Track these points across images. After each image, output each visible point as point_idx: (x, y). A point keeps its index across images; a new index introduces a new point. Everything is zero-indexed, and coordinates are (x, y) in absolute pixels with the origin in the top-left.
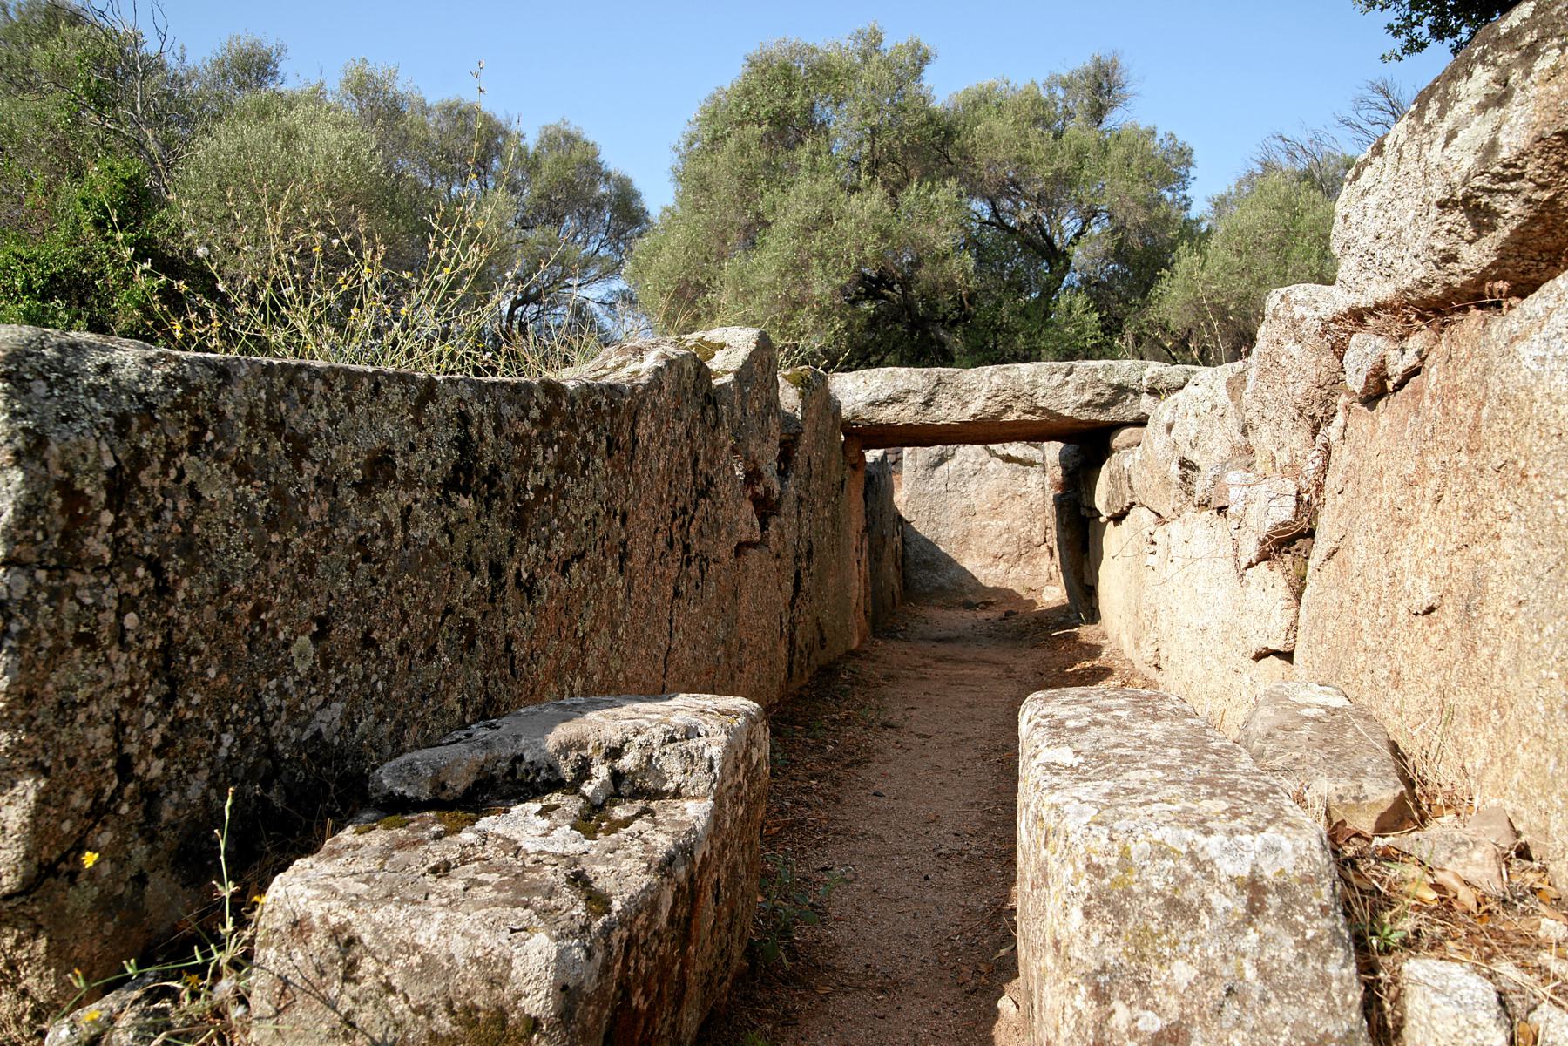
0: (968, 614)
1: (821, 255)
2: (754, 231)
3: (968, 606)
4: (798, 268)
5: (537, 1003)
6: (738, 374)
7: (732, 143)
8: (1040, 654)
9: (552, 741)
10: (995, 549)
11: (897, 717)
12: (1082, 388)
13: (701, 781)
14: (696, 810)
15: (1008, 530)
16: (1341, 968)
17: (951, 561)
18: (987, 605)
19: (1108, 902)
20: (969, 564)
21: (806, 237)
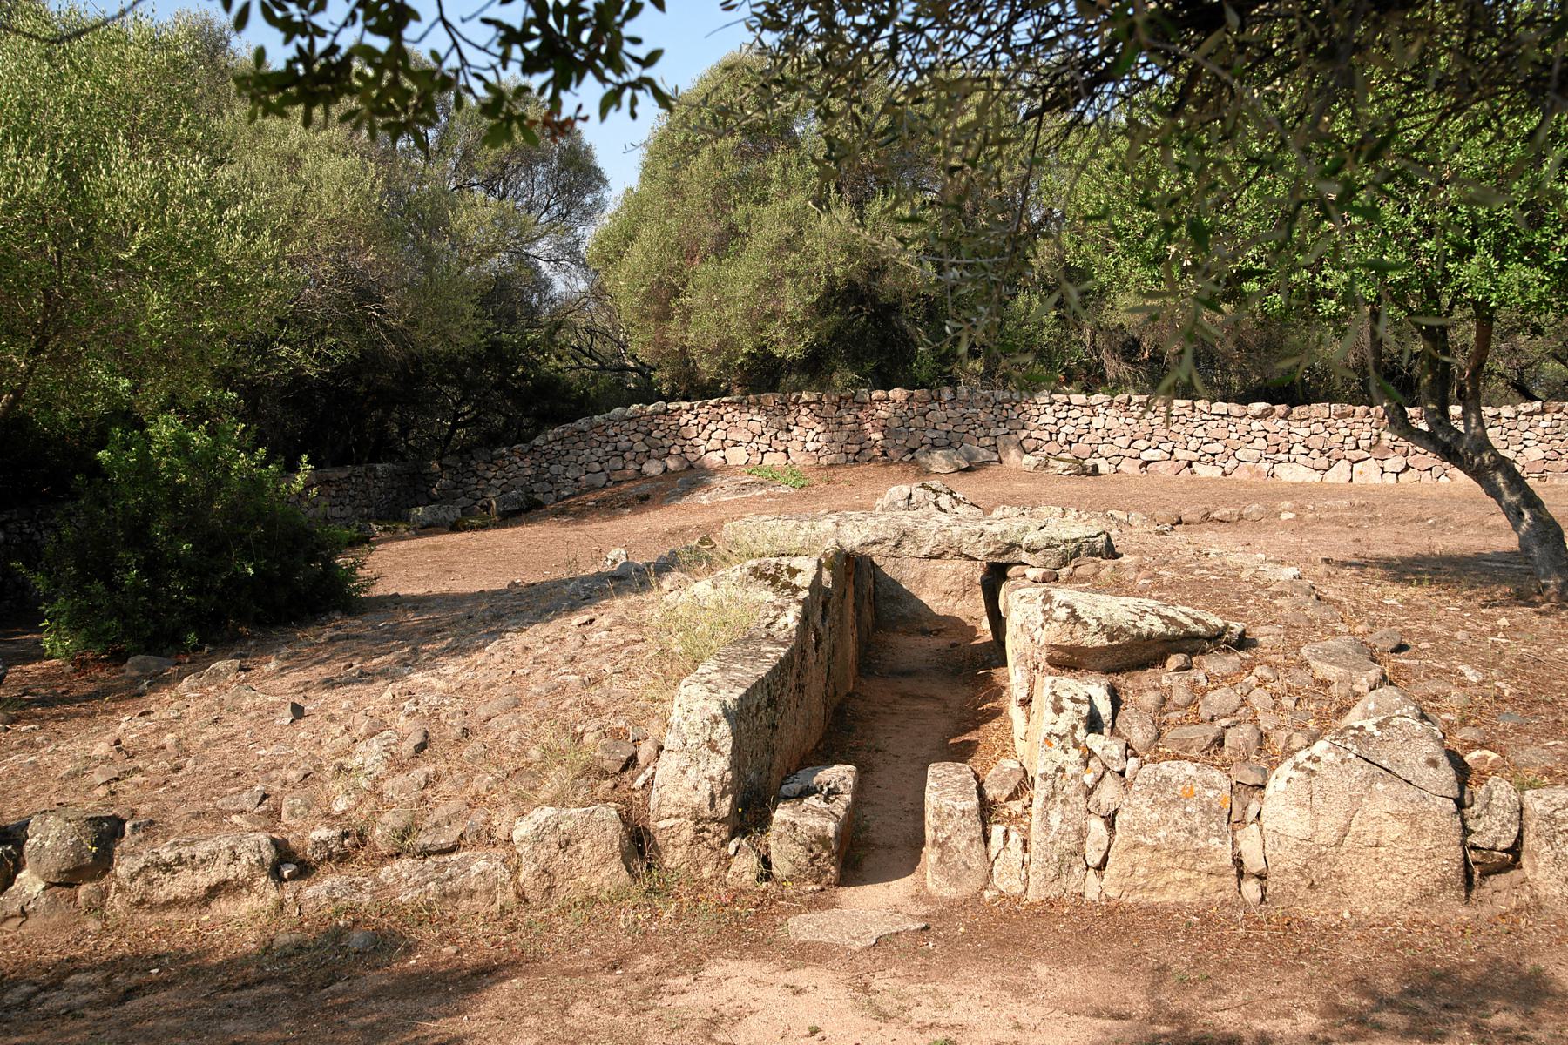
0: (924, 640)
1: (793, 274)
2: (729, 240)
3: (924, 632)
4: (772, 284)
5: (832, 835)
6: (811, 589)
7: (706, 152)
8: (967, 690)
9: (816, 780)
10: (945, 587)
11: (882, 744)
12: (988, 544)
13: (848, 790)
14: (848, 797)
15: (956, 572)
16: (979, 826)
17: (912, 596)
18: (938, 632)
19: (937, 814)
20: (925, 599)
21: (779, 257)
